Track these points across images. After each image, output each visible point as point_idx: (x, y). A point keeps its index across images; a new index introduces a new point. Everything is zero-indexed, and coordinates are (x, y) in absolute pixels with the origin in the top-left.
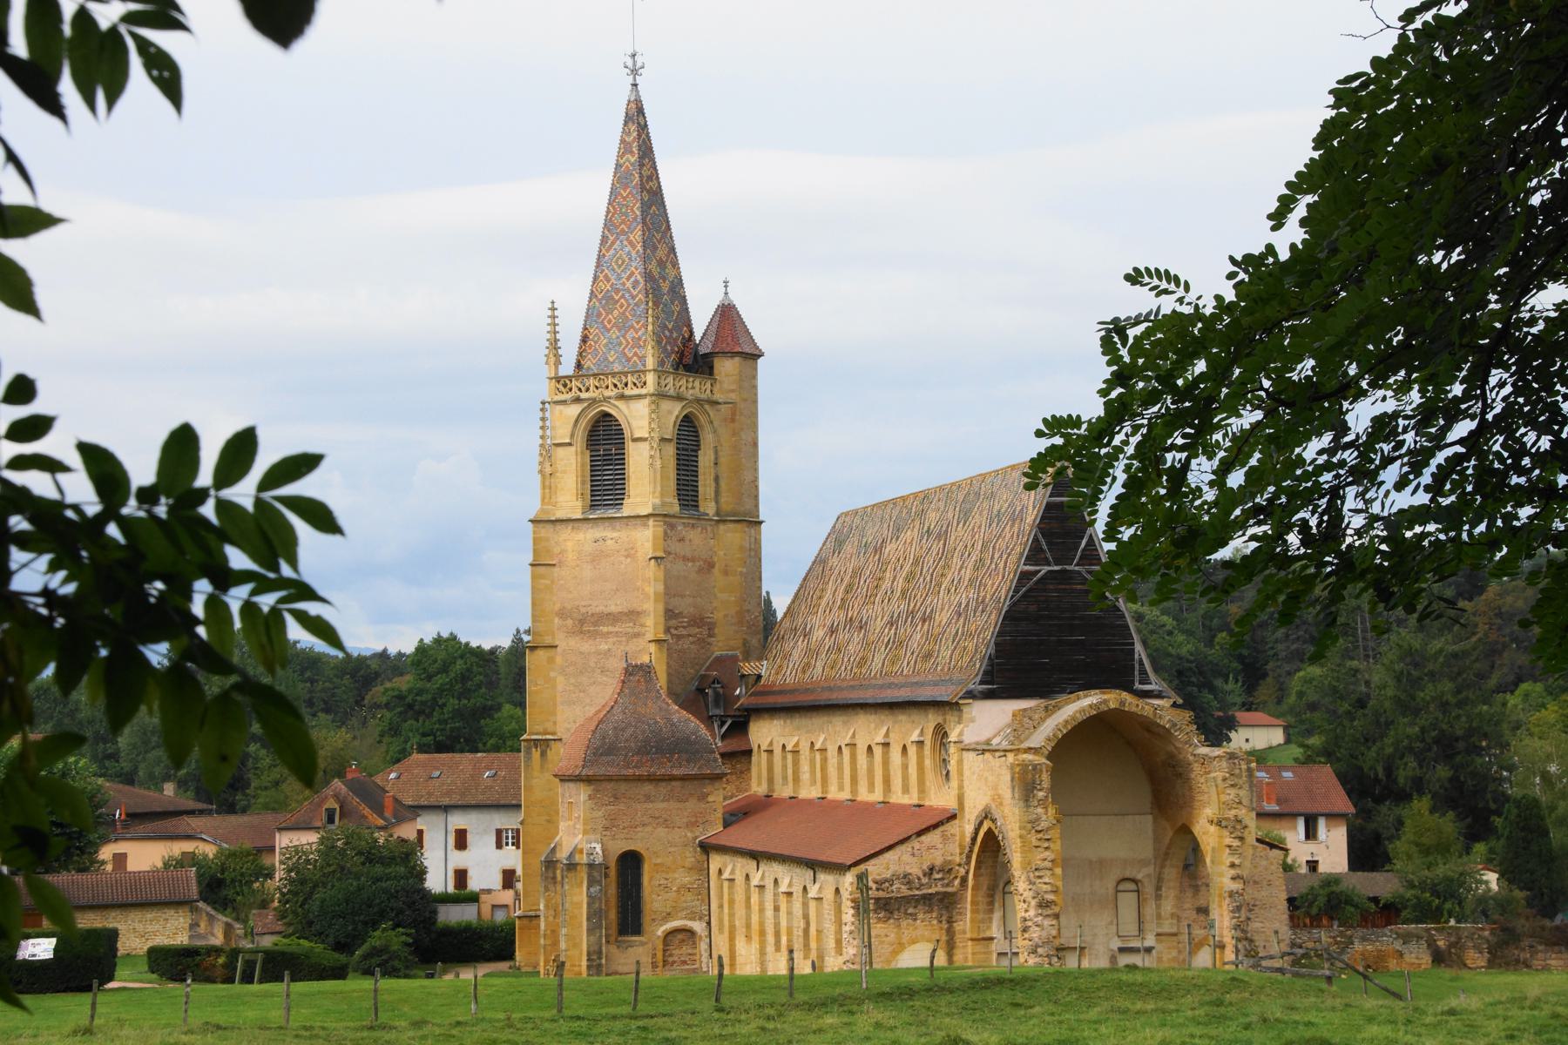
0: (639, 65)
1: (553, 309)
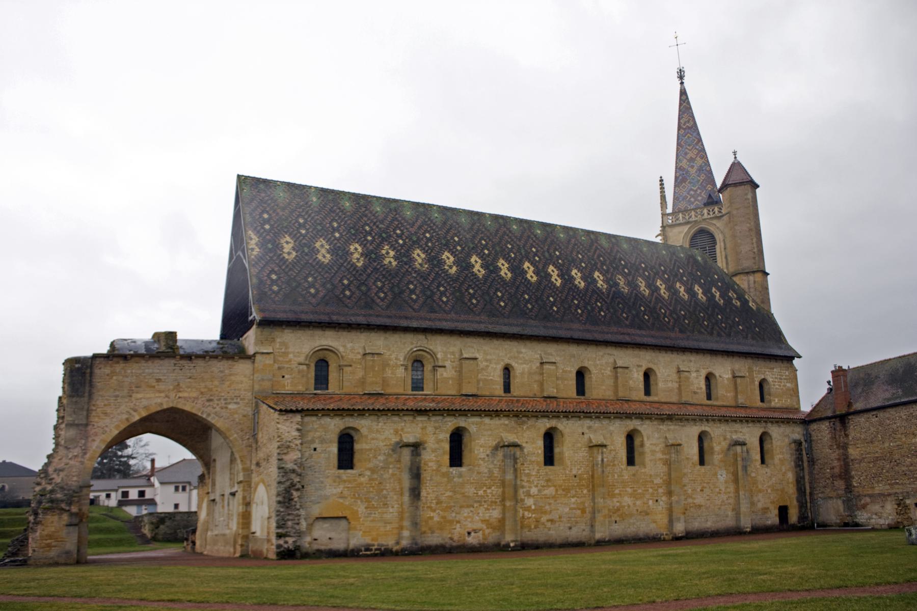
1: (661, 180)
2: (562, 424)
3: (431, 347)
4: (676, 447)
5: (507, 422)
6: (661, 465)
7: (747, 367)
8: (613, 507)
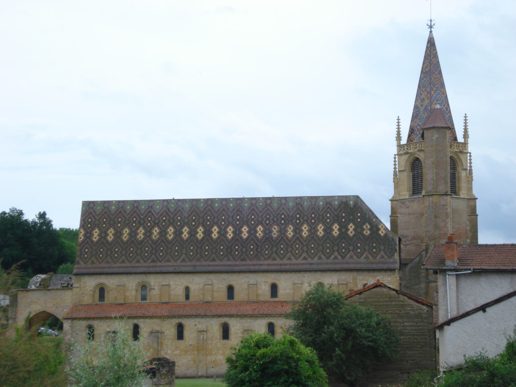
0: (432, 24)
1: (398, 119)
3: (148, 280)
4: (247, 331)
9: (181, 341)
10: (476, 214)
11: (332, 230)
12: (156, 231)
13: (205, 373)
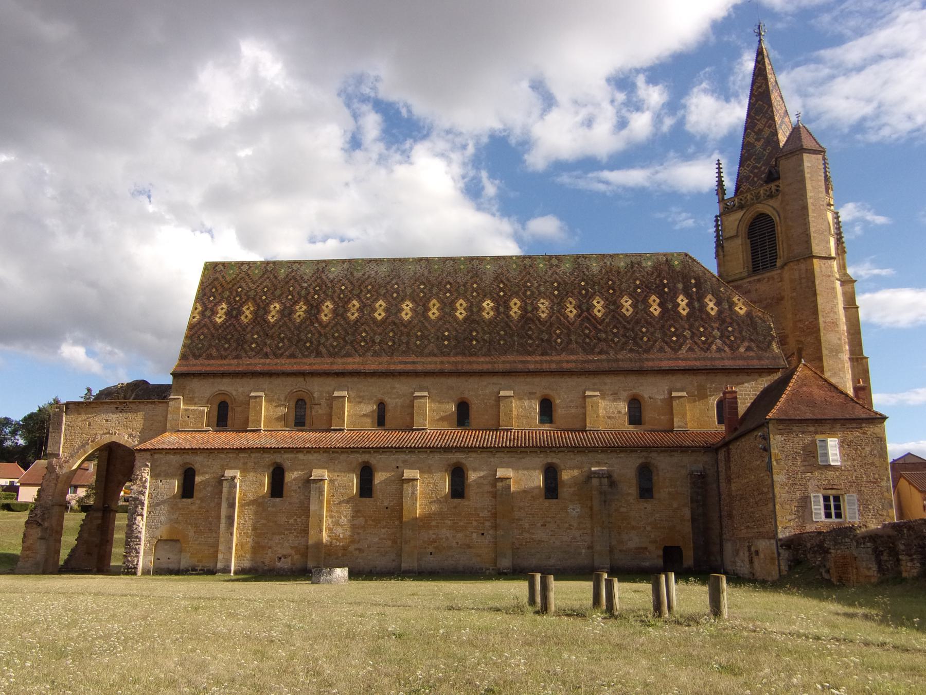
2: (375, 458)
3: (309, 388)
5: (319, 457)
6: (490, 498)
7: (696, 384)
8: (429, 539)
9: (367, 500)
10: (856, 305)
11: (648, 306)
12: (327, 307)
13: (416, 565)
